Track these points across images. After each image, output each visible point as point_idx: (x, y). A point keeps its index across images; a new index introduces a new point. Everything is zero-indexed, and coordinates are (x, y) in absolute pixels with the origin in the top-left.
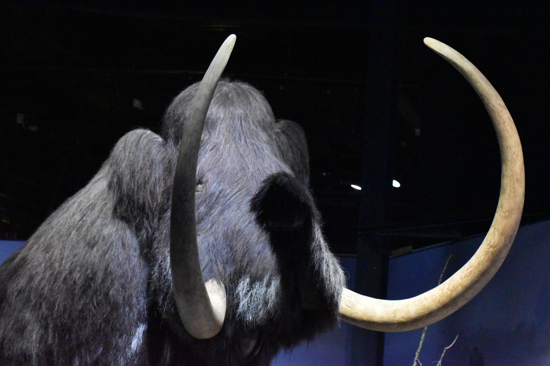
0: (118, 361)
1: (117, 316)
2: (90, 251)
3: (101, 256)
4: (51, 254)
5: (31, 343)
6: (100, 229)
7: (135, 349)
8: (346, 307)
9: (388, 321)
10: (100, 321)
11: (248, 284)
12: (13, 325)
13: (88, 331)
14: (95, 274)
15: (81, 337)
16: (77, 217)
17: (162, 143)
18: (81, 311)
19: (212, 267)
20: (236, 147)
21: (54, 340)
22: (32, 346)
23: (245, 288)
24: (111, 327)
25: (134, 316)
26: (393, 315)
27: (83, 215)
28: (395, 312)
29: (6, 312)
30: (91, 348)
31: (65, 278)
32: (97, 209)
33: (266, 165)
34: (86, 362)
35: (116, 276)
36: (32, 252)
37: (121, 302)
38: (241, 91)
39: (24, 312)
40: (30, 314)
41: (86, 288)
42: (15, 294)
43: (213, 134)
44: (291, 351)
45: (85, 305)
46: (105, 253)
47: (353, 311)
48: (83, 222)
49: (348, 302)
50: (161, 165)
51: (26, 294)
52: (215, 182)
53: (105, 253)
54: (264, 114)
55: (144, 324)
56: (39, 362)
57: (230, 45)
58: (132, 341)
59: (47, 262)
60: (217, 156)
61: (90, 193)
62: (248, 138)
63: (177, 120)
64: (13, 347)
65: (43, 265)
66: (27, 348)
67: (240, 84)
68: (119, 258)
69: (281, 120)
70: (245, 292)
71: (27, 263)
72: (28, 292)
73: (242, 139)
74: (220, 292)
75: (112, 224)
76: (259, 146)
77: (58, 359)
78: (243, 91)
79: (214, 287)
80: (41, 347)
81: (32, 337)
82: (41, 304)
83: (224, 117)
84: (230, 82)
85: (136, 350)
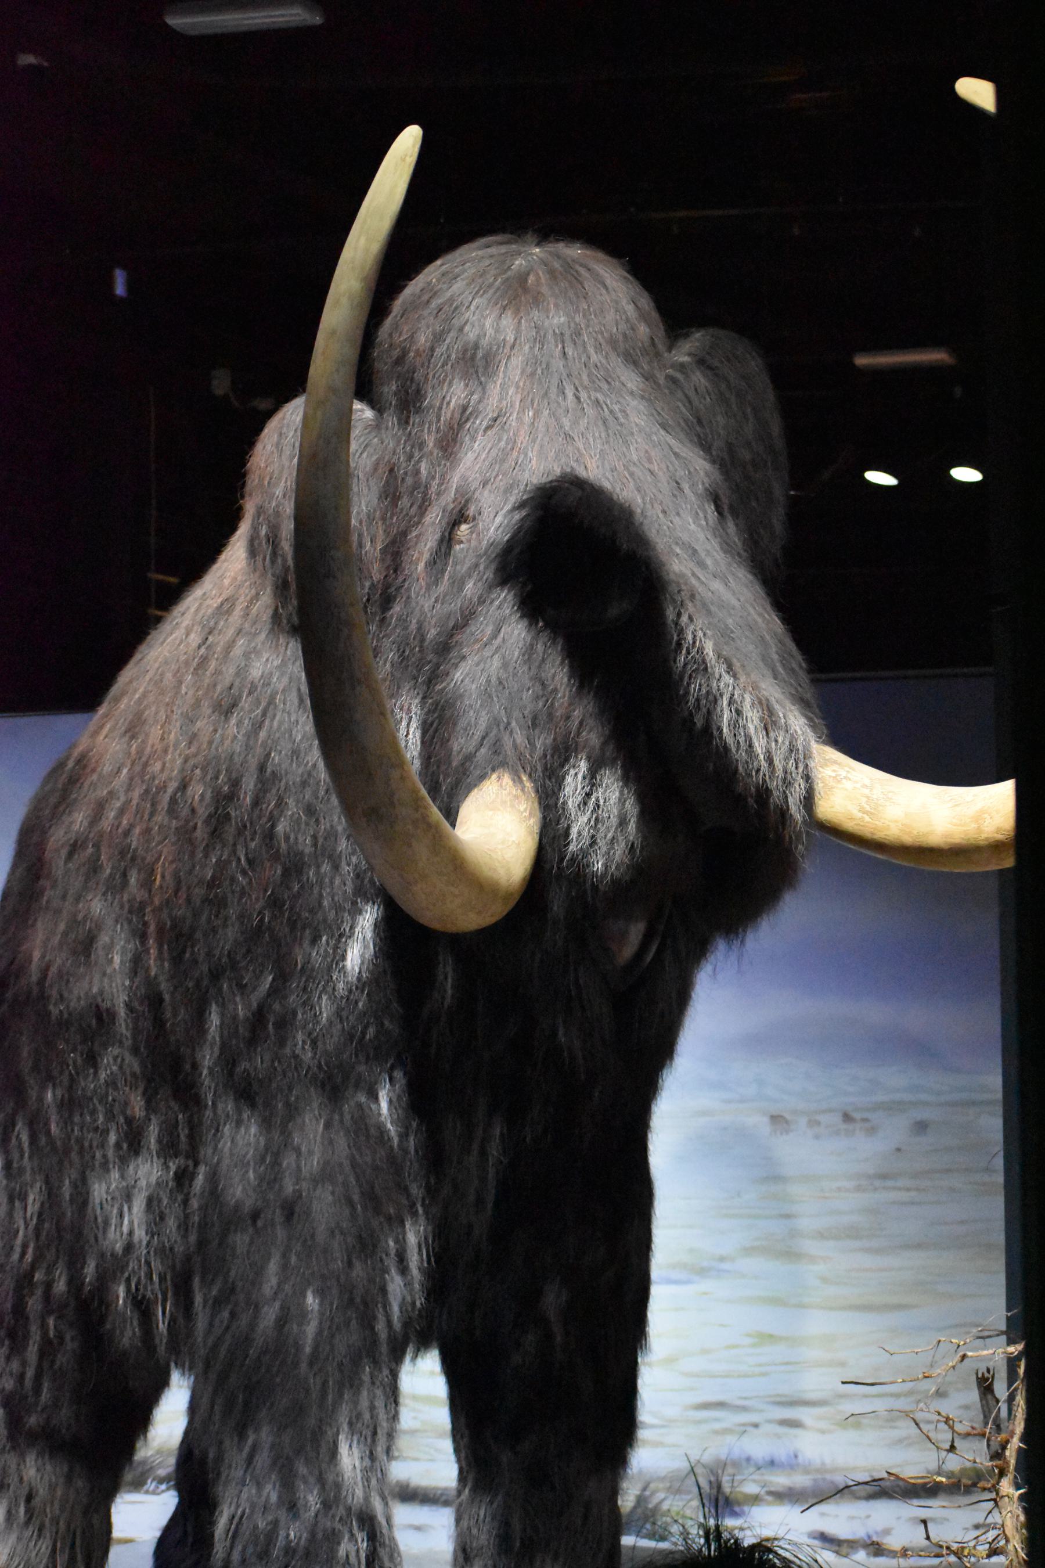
0: (312, 1007)
1: (302, 887)
2: (222, 724)
3: (248, 736)
4: (143, 742)
5: (111, 977)
6: (243, 664)
7: (357, 970)
8: (860, 815)
9: (964, 842)
10: (258, 907)
11: (584, 778)
12: (65, 934)
13: (231, 935)
14: (235, 784)
15: (217, 952)
16: (195, 639)
17: (373, 423)
18: (212, 884)
19: (498, 741)
20: (553, 414)
21: (162, 965)
22: (114, 985)
23: (579, 787)
24: (289, 919)
25: (345, 885)
26: (974, 826)
27: (207, 630)
28: (978, 818)
29: (48, 902)
30: (243, 978)
31: (173, 801)
32: (238, 612)
33: (635, 457)
34: (235, 1017)
35: (287, 783)
36: (101, 738)
37: (308, 850)
38: (562, 266)
39: (89, 898)
40: (103, 903)
41: (218, 821)
42: (64, 853)
43: (490, 386)
44: (743, 942)
45: (222, 866)
46: (258, 726)
47: (877, 822)
48: (207, 649)
49: (865, 799)
50: (372, 483)
51: (90, 850)
52: (500, 513)
53: (258, 726)
54: (627, 320)
55: (374, 903)
56: (136, 1021)
57: (406, 155)
58: (346, 951)
59: (133, 764)
60: (502, 444)
61: (225, 571)
62: (585, 388)
63: (400, 361)
64: (71, 992)
65: (125, 771)
66: (101, 992)
67: (561, 246)
68: (293, 736)
69: (694, 330)
70: (580, 798)
71: (88, 770)
72: (93, 846)
73: (567, 391)
74: (520, 803)
75: (270, 647)
76: (616, 408)
77: (175, 1015)
78: (568, 266)
79: (504, 792)
80: (135, 985)
81: (111, 961)
82: (124, 875)
83: (516, 340)
84: (538, 245)
85: (360, 973)
